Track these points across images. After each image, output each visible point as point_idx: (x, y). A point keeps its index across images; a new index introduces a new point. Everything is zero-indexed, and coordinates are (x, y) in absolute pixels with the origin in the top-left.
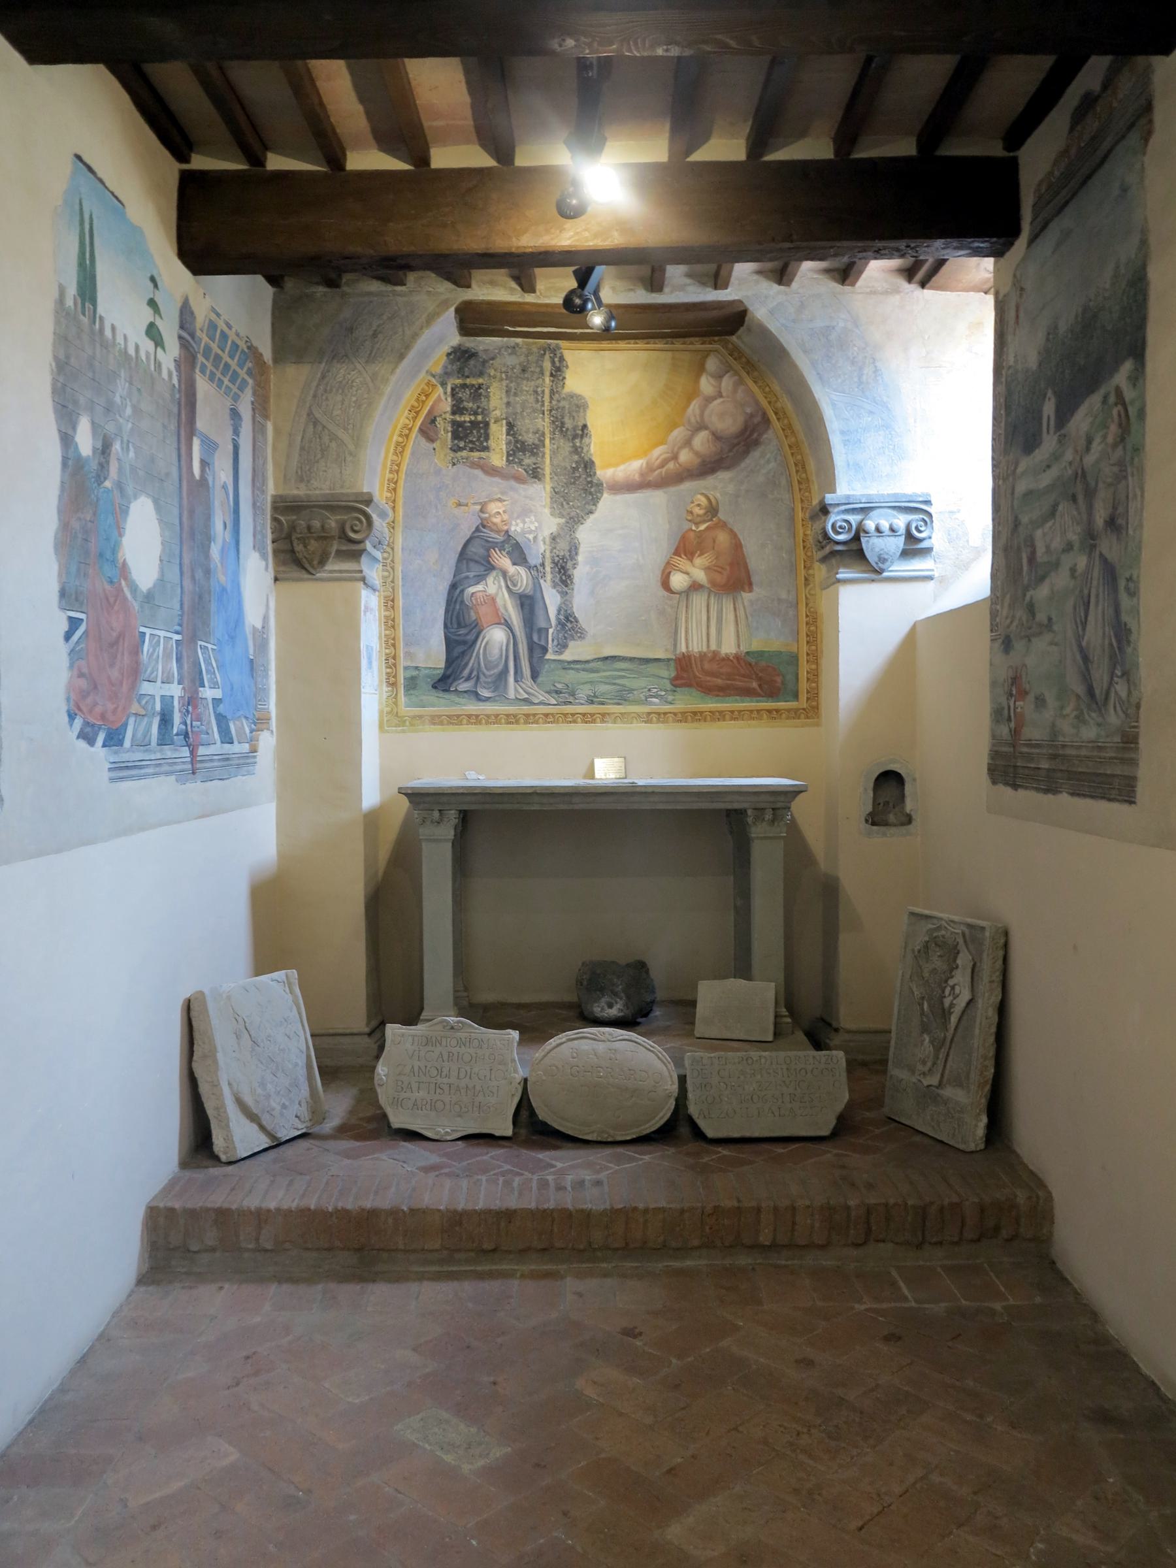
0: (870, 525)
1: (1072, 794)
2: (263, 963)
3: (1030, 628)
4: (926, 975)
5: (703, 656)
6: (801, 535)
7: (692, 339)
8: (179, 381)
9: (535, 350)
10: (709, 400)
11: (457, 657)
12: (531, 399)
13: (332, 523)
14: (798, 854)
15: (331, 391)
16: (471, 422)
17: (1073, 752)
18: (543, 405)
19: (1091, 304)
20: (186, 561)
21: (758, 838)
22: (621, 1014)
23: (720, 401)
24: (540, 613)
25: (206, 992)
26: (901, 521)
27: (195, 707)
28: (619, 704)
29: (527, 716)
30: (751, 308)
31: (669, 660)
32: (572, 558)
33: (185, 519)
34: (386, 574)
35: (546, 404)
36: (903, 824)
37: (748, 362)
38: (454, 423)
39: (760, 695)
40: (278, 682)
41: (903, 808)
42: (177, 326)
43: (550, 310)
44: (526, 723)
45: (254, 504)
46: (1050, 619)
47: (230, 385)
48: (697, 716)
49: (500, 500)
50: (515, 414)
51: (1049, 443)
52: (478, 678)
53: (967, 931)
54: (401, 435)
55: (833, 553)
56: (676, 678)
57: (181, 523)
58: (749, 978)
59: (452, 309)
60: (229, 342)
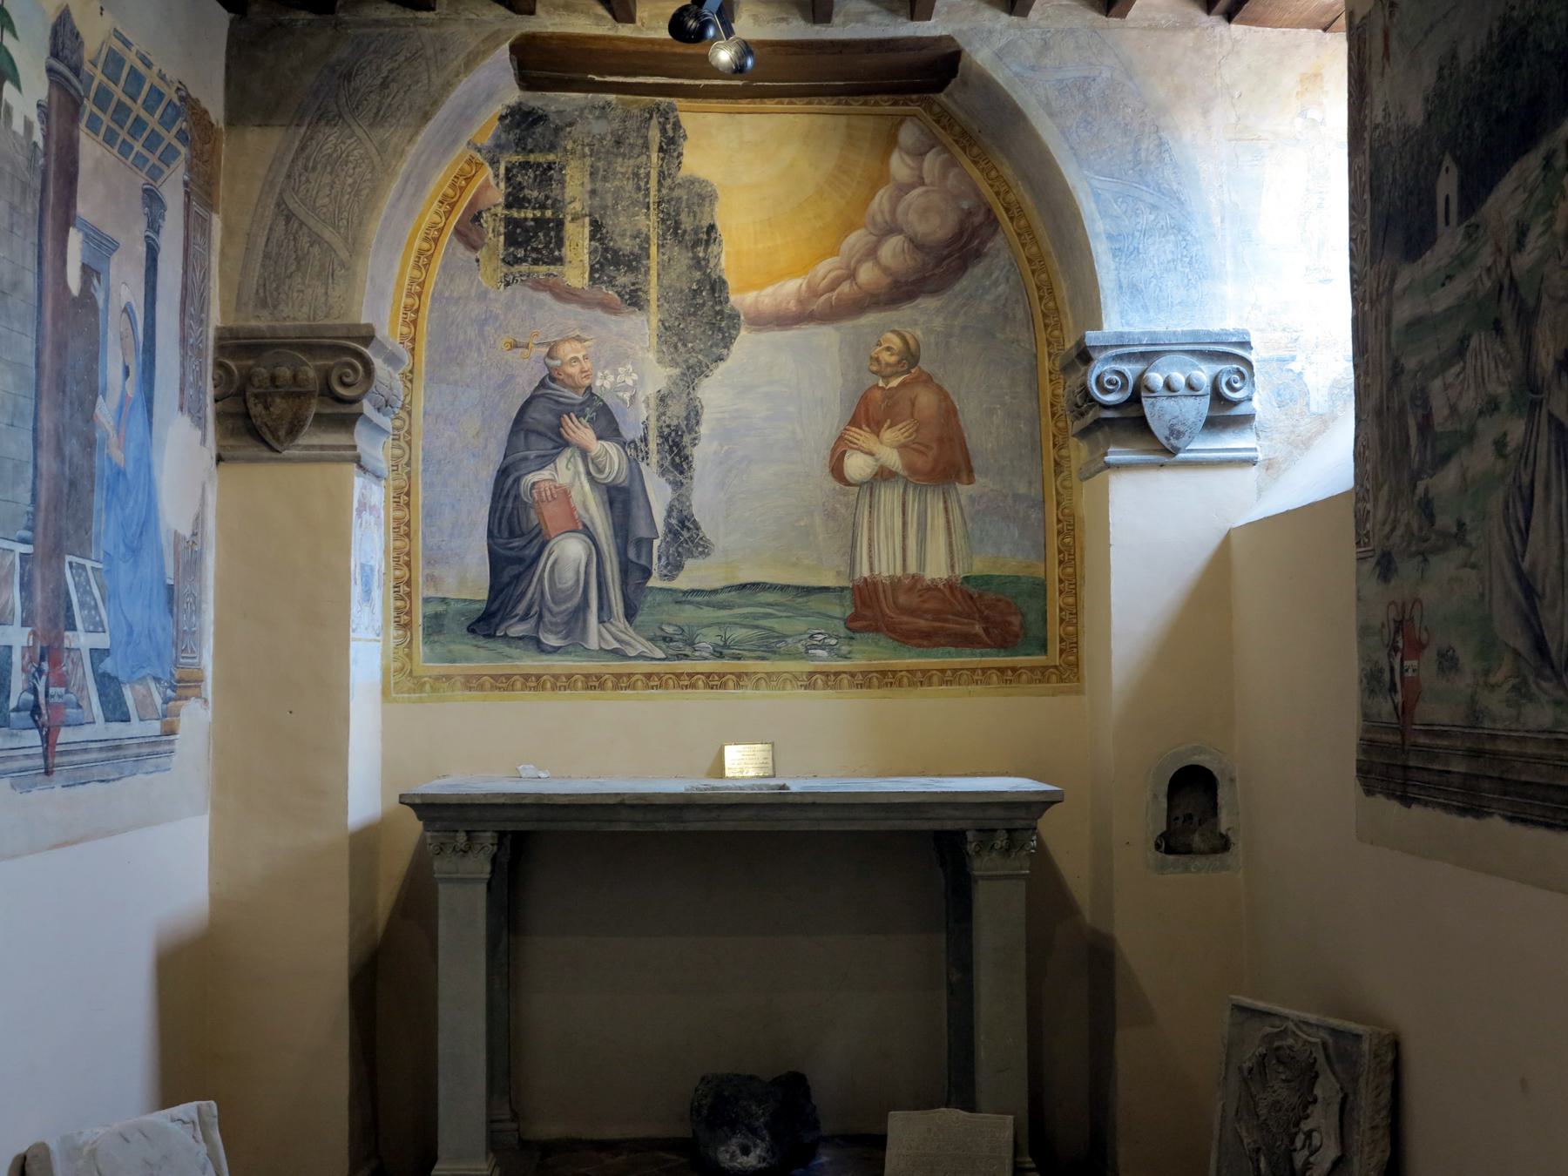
0: (1156, 378)
1: (1512, 819)
2: (169, 1093)
3: (1426, 540)
4: (1263, 1112)
5: (895, 583)
6: (1049, 395)
7: (878, 97)
8: (46, 137)
9: (636, 112)
10: (904, 189)
11: (509, 584)
12: (630, 186)
13: (311, 370)
14: (1047, 895)
15: (314, 169)
16: (535, 219)
17: (1513, 748)
18: (647, 195)
19: (1515, 14)
20: (47, 423)
21: (983, 878)
22: (763, 1165)
23: (920, 191)
24: (639, 514)
25: (53, 1145)
26: (1204, 374)
27: (56, 663)
28: (763, 659)
29: (618, 676)
30: (967, 49)
31: (842, 589)
32: (691, 430)
33: (47, 357)
34: (398, 452)
35: (653, 192)
36: (1214, 851)
37: (964, 133)
38: (509, 221)
39: (986, 646)
40: (218, 621)
41: (1216, 824)
42: (46, 53)
43: (657, 48)
44: (616, 687)
45: (183, 340)
46: (1461, 525)
47: (145, 153)
48: (887, 678)
49: (578, 339)
50: (605, 207)
51: (1449, 241)
52: (541, 617)
53: (1330, 1041)
54: (426, 239)
55: (1099, 423)
56: (855, 617)
57: (38, 365)
58: (970, 1106)
59: (506, 46)
60: (146, 88)
